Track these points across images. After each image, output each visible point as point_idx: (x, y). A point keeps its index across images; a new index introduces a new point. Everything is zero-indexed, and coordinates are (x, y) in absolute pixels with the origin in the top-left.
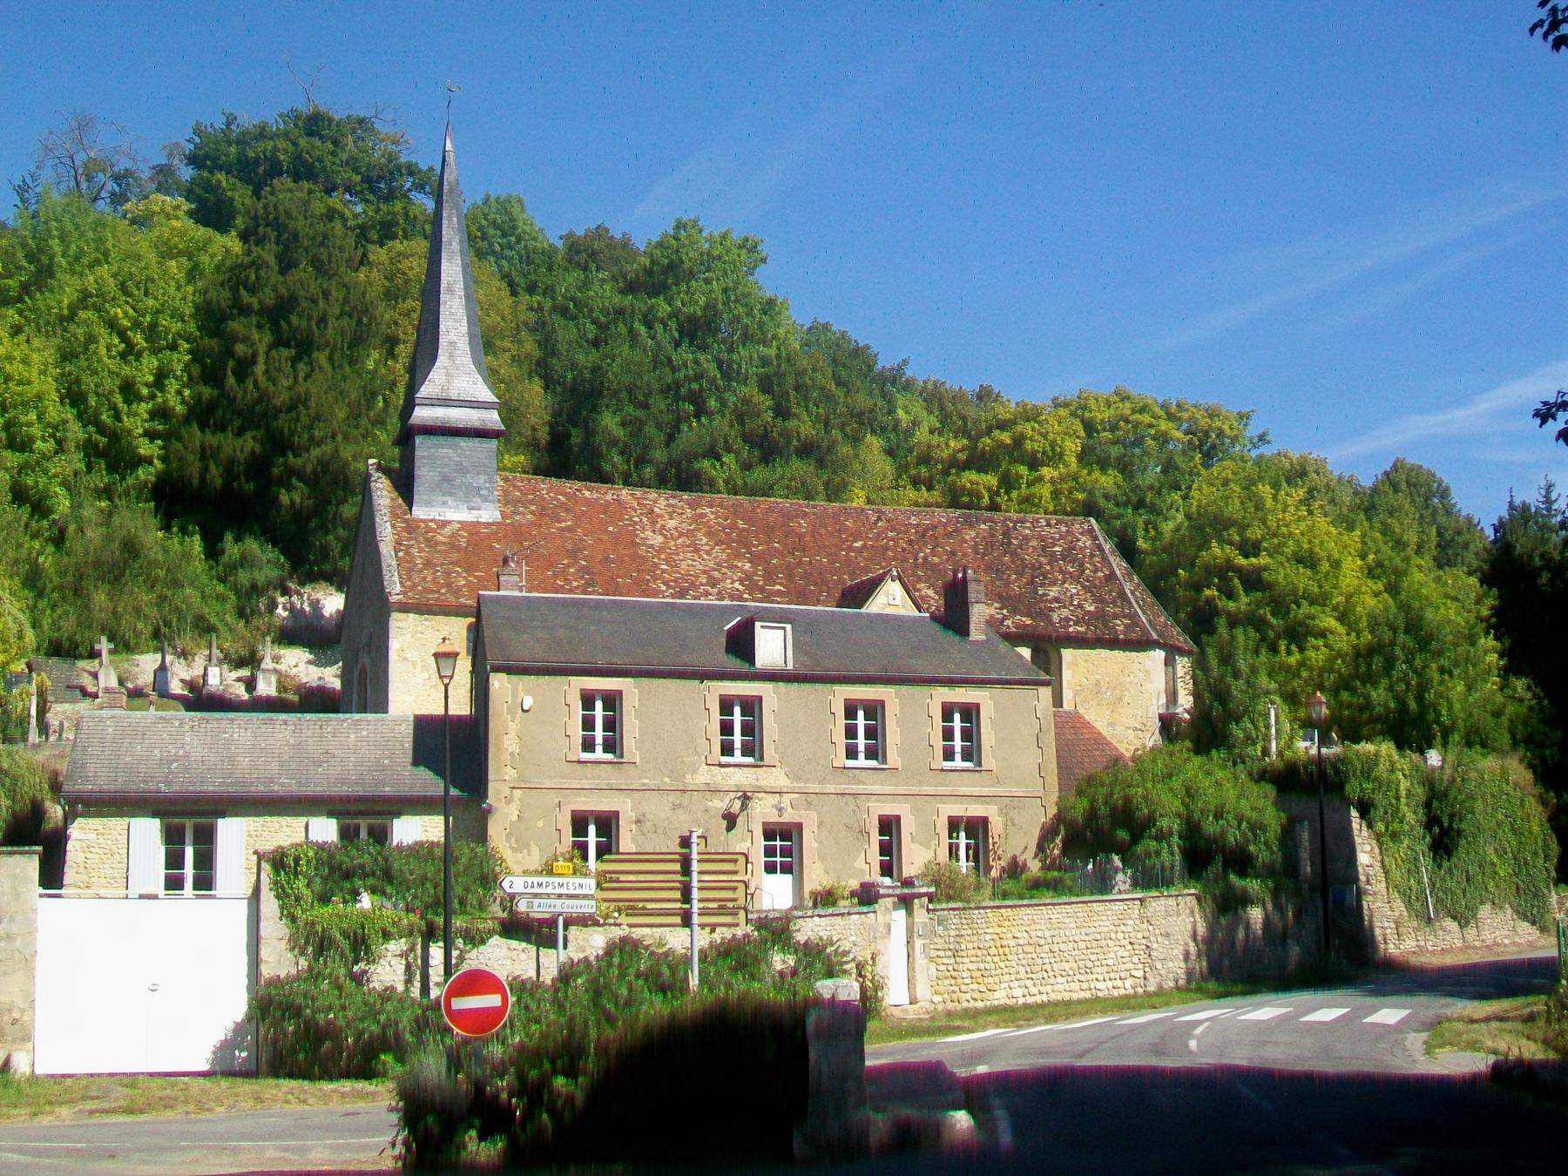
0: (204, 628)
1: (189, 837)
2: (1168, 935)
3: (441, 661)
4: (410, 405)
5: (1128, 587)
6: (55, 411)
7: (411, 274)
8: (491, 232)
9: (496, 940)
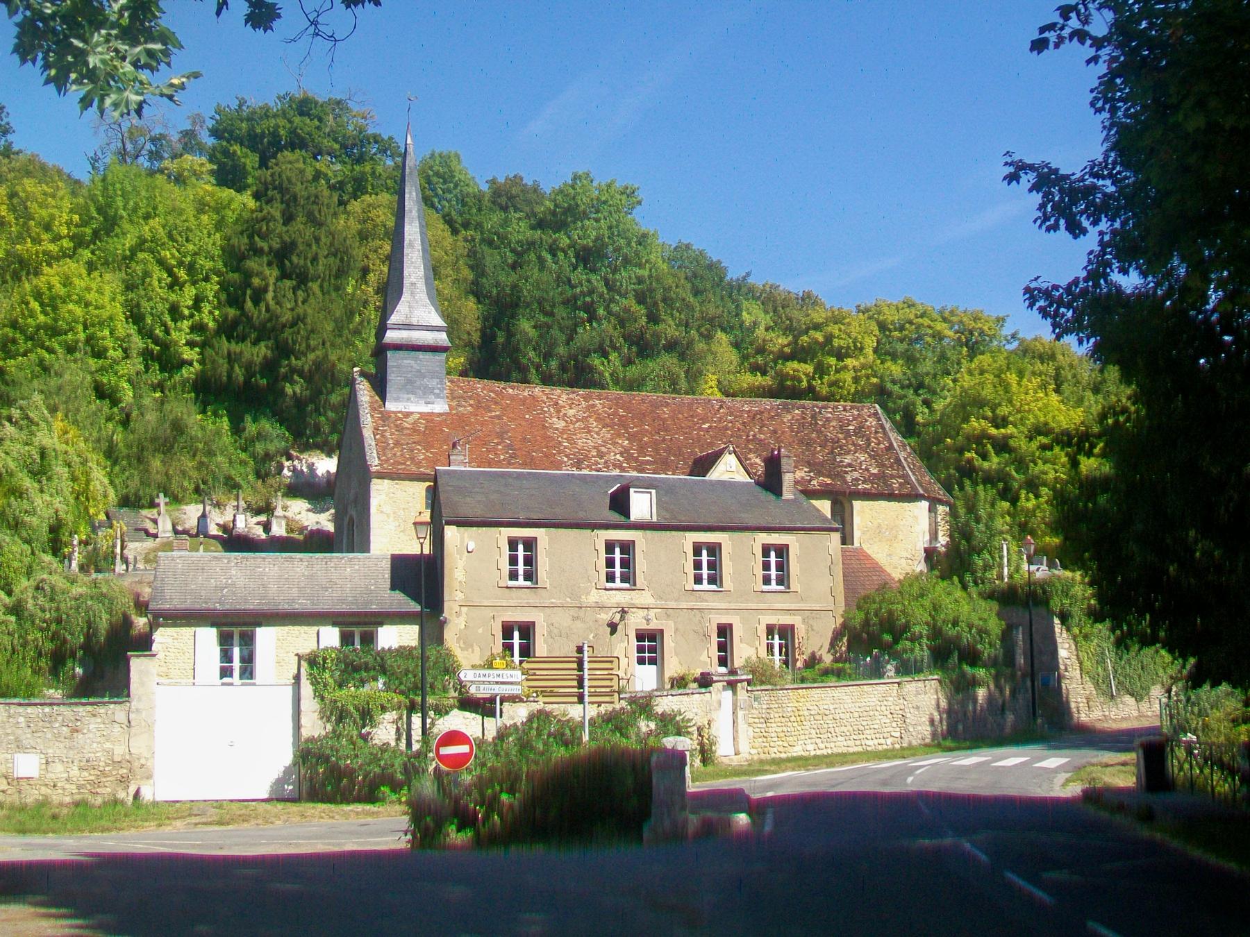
0: (232, 485)
1: (236, 639)
2: (918, 708)
3: (419, 528)
4: (382, 329)
5: (902, 455)
6: (124, 328)
7: (378, 220)
8: (435, 179)
9: (455, 712)
